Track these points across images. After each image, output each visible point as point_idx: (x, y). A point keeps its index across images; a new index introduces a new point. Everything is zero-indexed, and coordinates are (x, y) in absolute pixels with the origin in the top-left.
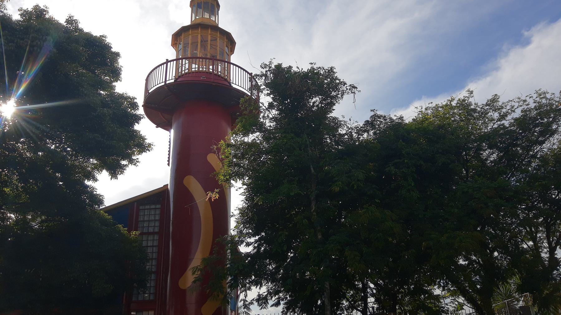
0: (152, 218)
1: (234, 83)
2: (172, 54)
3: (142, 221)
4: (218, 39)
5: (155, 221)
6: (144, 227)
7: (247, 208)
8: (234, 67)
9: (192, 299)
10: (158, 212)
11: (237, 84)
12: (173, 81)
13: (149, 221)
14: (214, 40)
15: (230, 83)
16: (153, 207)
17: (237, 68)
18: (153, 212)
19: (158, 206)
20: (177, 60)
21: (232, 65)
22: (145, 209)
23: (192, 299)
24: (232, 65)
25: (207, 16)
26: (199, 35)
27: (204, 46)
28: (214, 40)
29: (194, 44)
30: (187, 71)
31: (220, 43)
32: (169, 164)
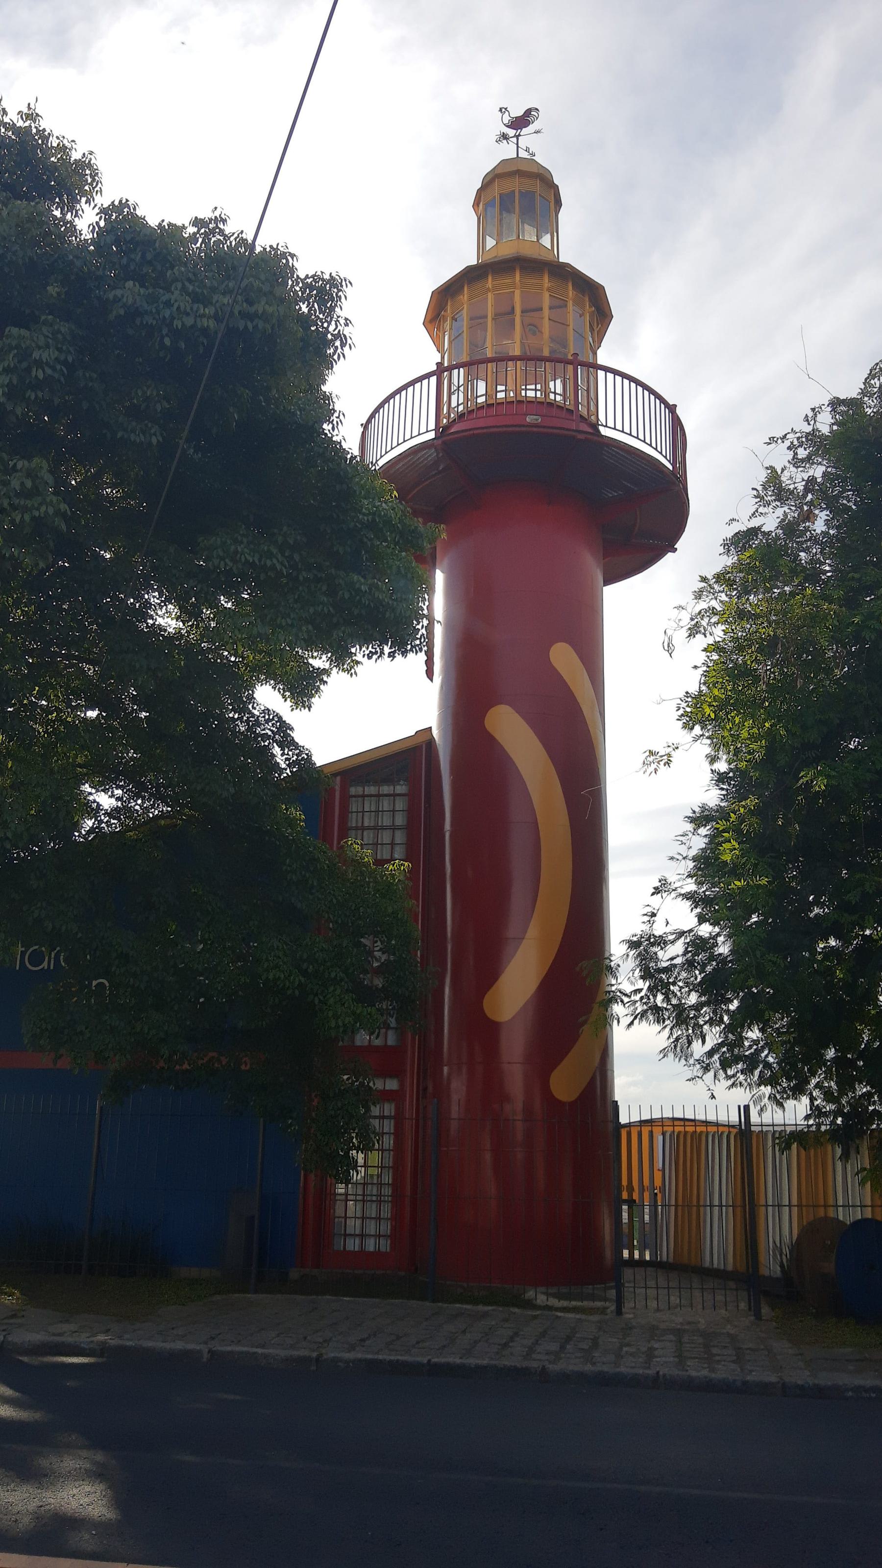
0: (386, 821)
1: (611, 423)
2: (427, 356)
3: (357, 828)
4: (570, 304)
5: (393, 828)
6: (378, 1219)
7: (319, 386)
8: (610, 376)
9: (514, 1048)
10: (400, 804)
11: (619, 427)
12: (432, 435)
13: (377, 828)
14: (559, 305)
15: (595, 426)
16: (386, 789)
17: (626, 382)
18: (386, 804)
19: (401, 789)
20: (440, 371)
21: (601, 374)
22: (363, 796)
23: (514, 1048)
24: (601, 374)
25: (530, 234)
26: (517, 293)
27: (532, 329)
28: (559, 305)
29: (505, 316)
30: (481, 400)
31: (576, 316)
32: (430, 674)
